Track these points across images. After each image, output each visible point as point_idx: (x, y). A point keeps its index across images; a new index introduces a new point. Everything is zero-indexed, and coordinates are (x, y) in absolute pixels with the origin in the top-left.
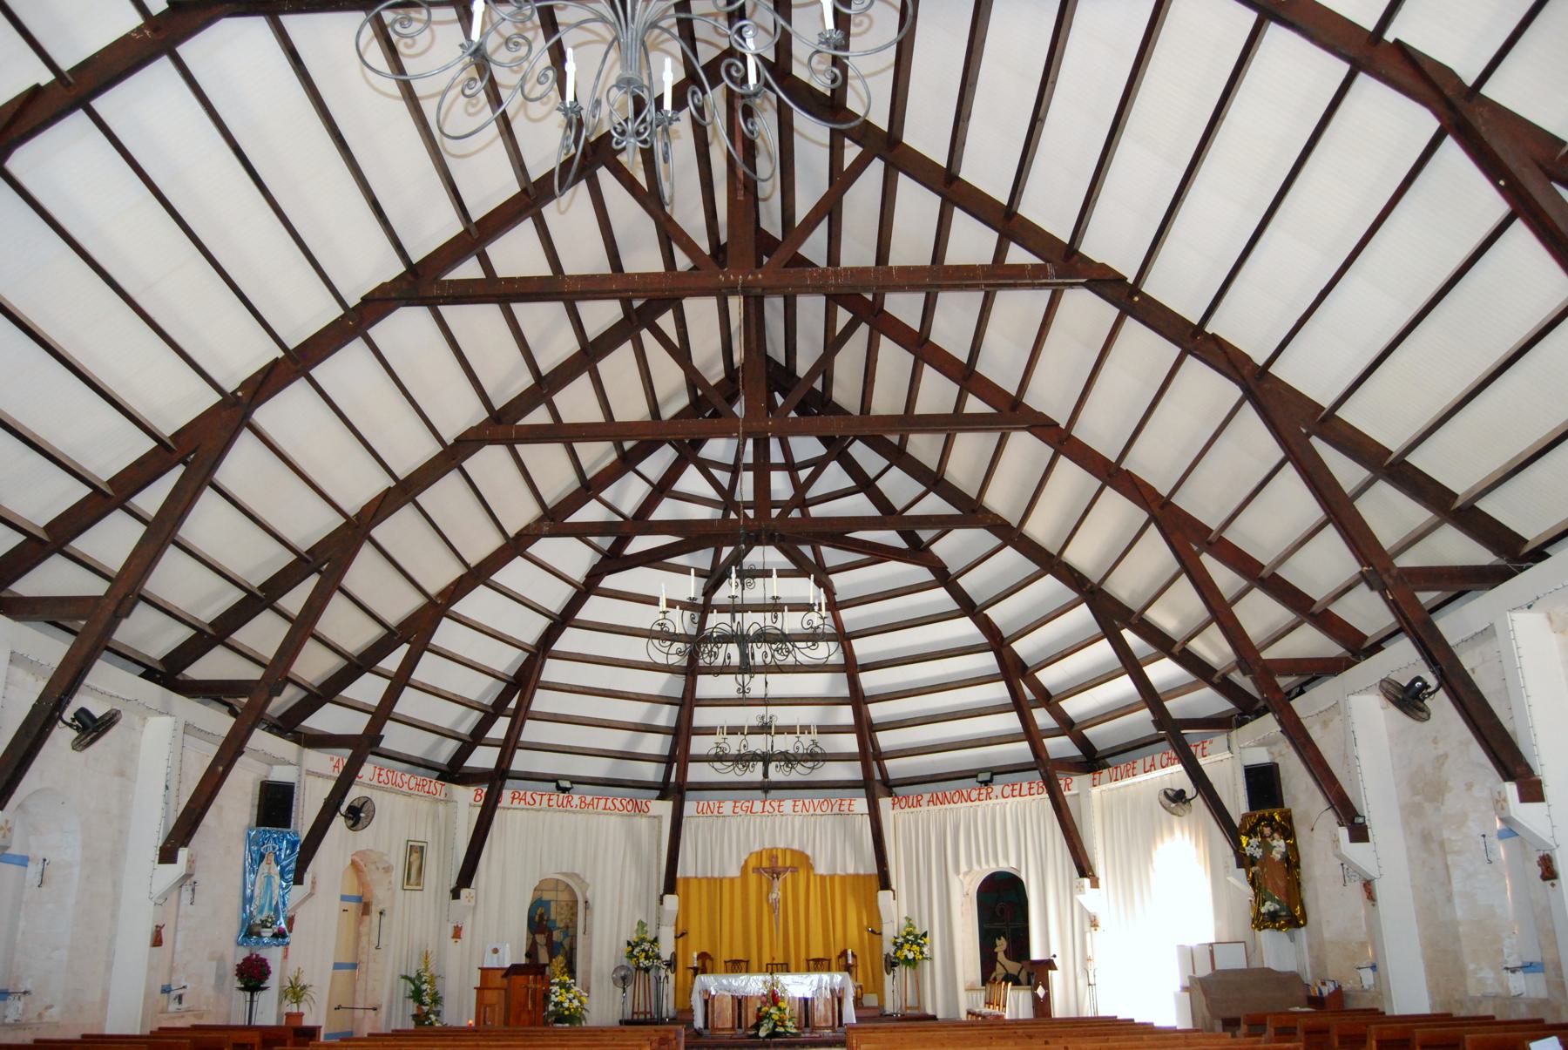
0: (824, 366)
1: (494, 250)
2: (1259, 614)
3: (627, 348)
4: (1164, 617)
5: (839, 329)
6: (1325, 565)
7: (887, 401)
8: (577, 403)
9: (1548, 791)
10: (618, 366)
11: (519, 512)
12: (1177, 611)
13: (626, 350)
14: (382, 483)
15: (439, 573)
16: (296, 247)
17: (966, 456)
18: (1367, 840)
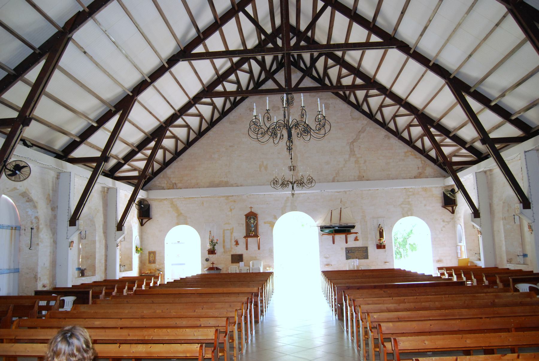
0: (312, 26)
1: (208, 42)
2: (488, 118)
3: (233, 20)
4: (449, 123)
5: (318, 11)
6: (468, 133)
7: (338, 37)
8: (214, 43)
9: (481, 215)
10: (230, 27)
11: (195, 88)
12: (455, 119)
13: (233, 22)
14: (172, 112)
15: (165, 113)
16: (180, 89)
17: (369, 61)
18: (530, 208)
